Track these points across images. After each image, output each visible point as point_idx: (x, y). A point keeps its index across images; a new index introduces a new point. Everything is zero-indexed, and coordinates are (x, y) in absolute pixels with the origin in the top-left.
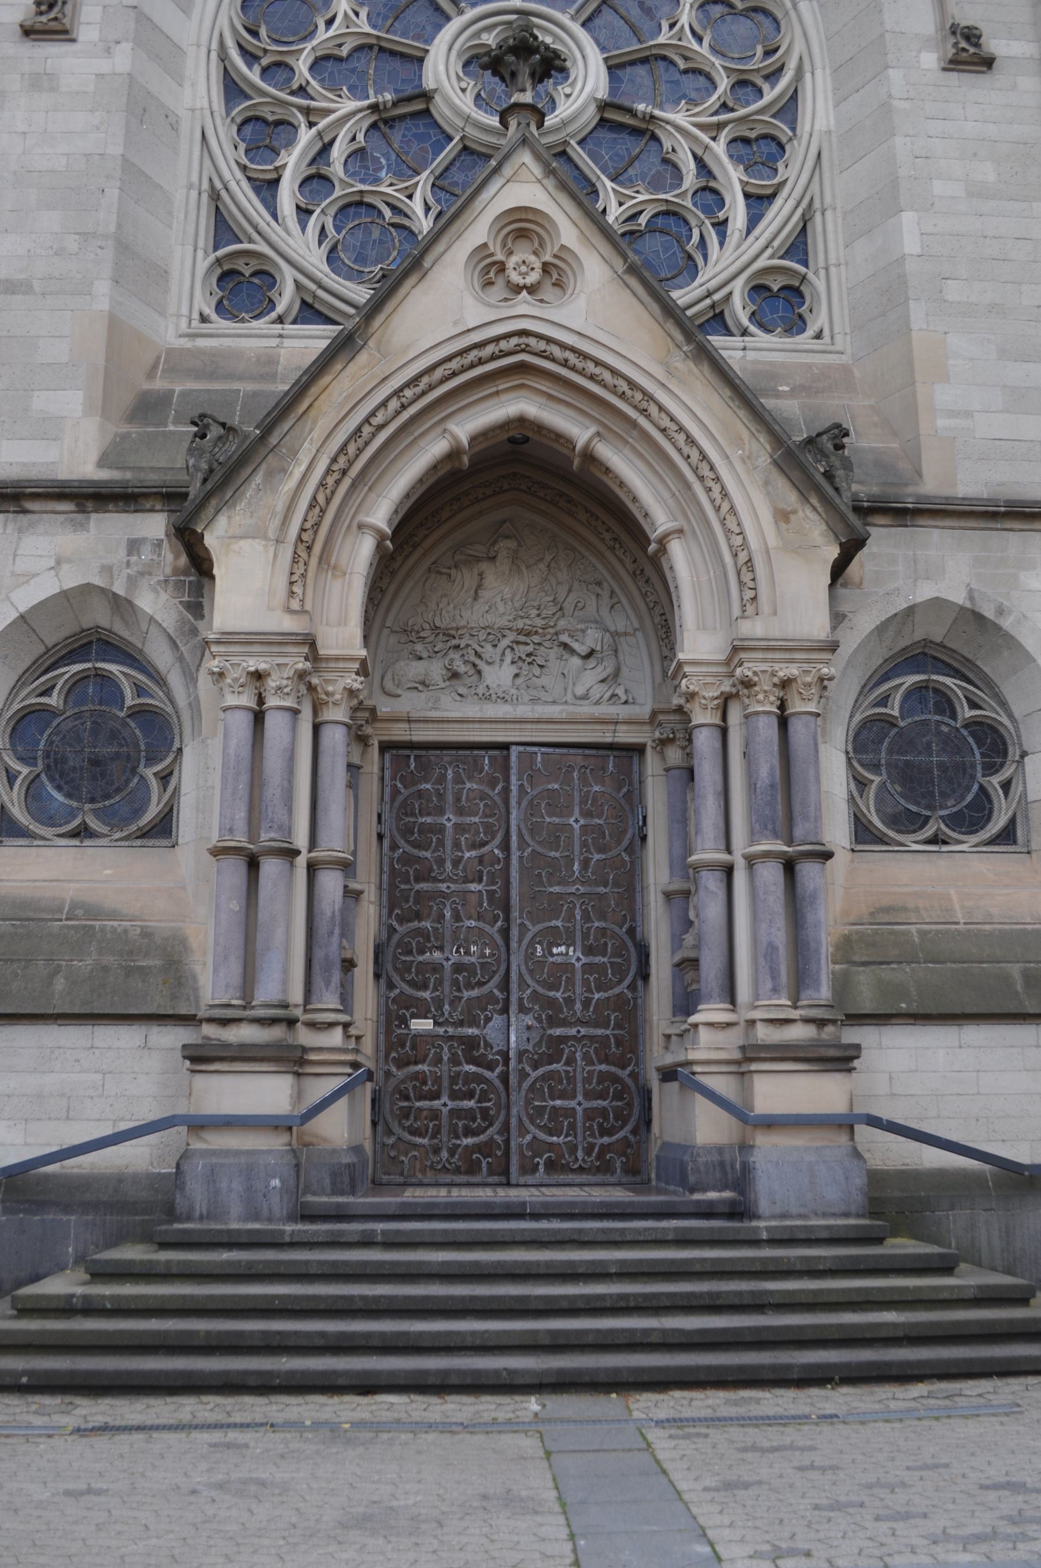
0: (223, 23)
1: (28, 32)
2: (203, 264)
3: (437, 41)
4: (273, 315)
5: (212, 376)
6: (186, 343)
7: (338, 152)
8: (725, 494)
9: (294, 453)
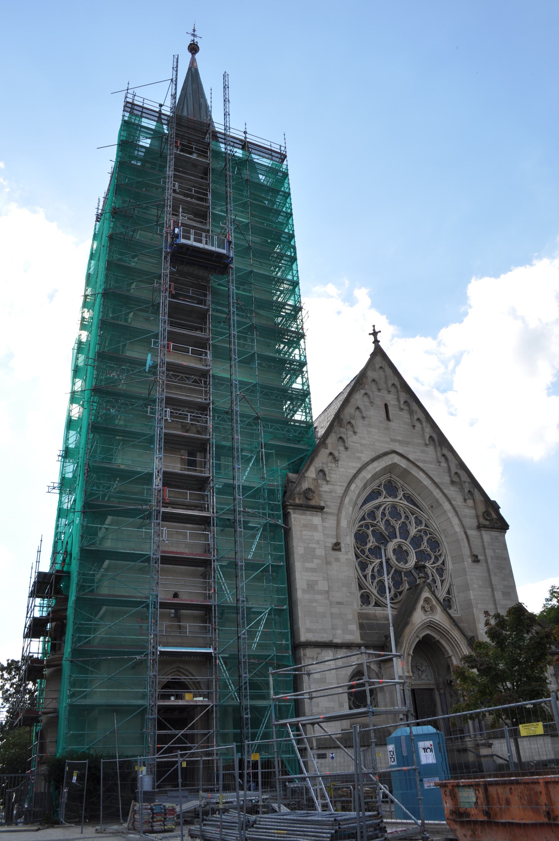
1: (333, 549)
7: (376, 570)
8: (461, 649)
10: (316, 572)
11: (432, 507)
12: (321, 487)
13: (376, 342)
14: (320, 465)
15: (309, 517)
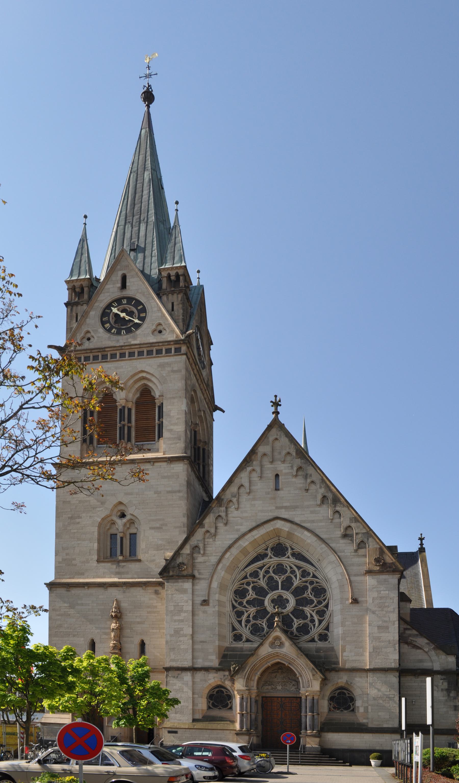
0: (231, 596)
2: (231, 635)
3: (266, 598)
4: (242, 641)
5: (233, 651)
6: (229, 646)
9: (246, 668)
10: (183, 622)
11: (319, 560)
12: (197, 559)
13: (276, 413)
14: (196, 542)
15: (180, 584)
